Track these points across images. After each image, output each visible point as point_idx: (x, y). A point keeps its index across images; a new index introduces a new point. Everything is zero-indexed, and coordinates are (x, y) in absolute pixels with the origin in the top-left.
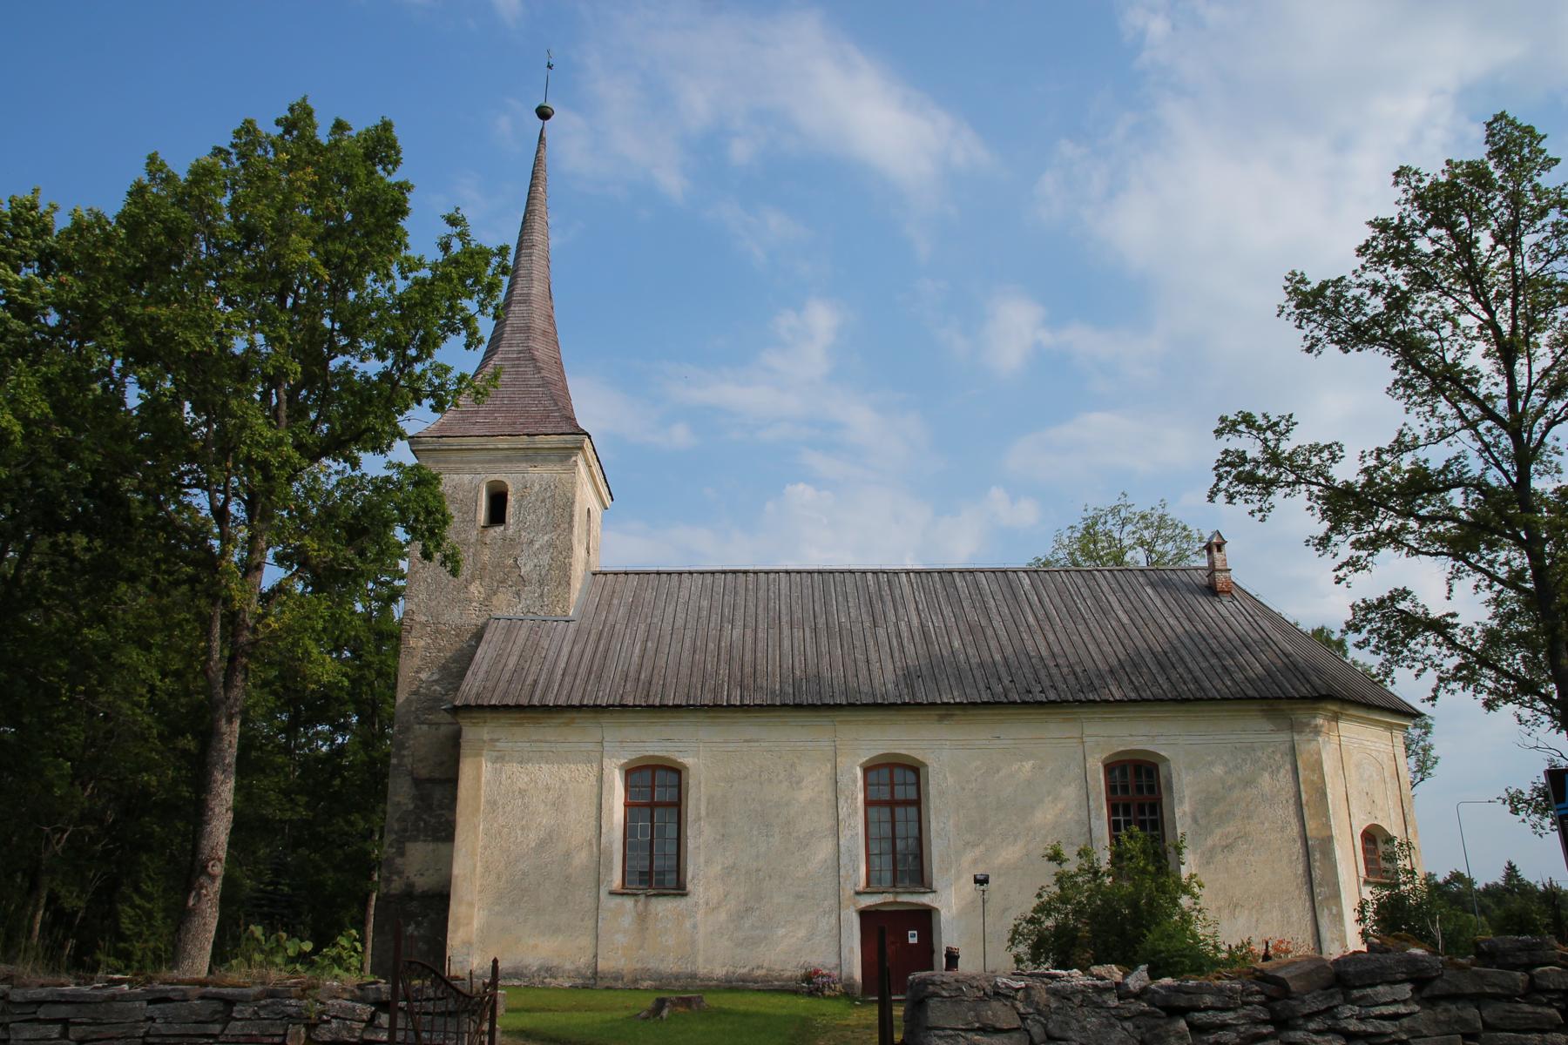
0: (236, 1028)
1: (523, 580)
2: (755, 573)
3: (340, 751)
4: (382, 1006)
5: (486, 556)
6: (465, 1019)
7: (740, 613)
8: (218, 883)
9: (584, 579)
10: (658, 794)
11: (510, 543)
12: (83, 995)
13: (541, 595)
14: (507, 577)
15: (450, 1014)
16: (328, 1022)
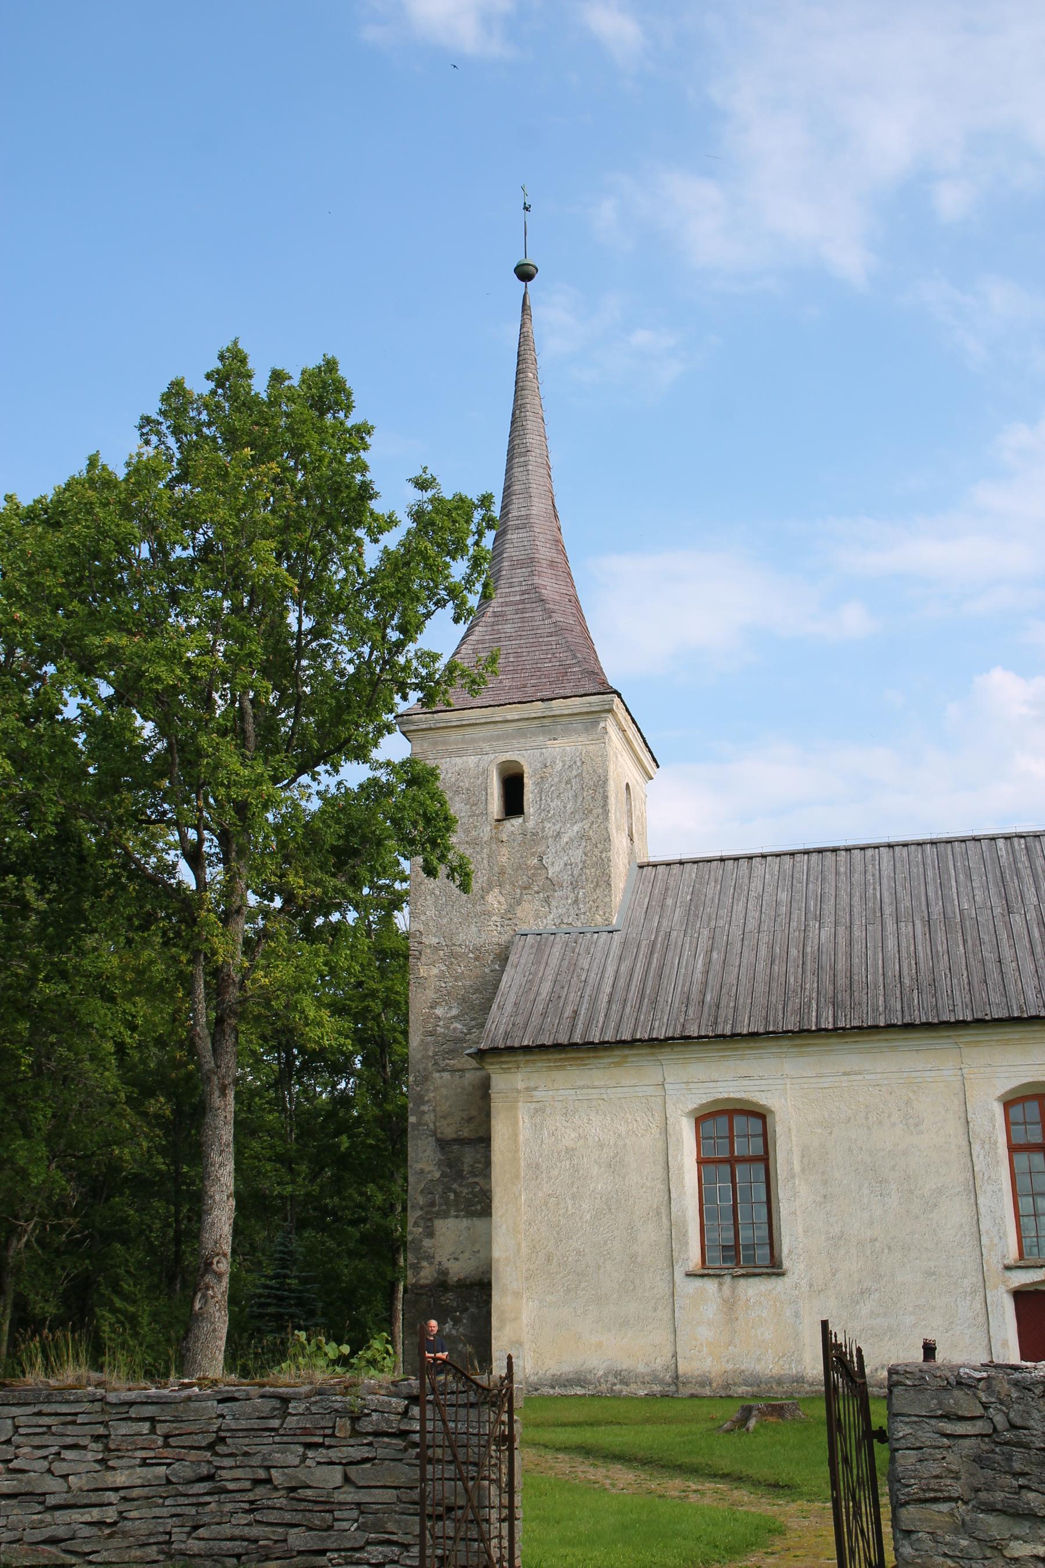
0: (291, 1422)
1: (552, 884)
2: (848, 850)
3: (343, 1101)
4: (414, 1399)
5: (504, 857)
6: (485, 1409)
7: (829, 906)
8: (225, 1281)
9: (629, 875)
10: (738, 1146)
11: (532, 839)
12: (166, 1397)
13: (576, 901)
14: (533, 881)
15: (472, 1405)
16: (368, 1415)
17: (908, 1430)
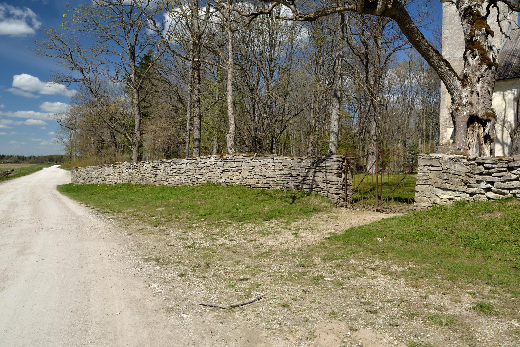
0: (303, 164)
17: (421, 168)
